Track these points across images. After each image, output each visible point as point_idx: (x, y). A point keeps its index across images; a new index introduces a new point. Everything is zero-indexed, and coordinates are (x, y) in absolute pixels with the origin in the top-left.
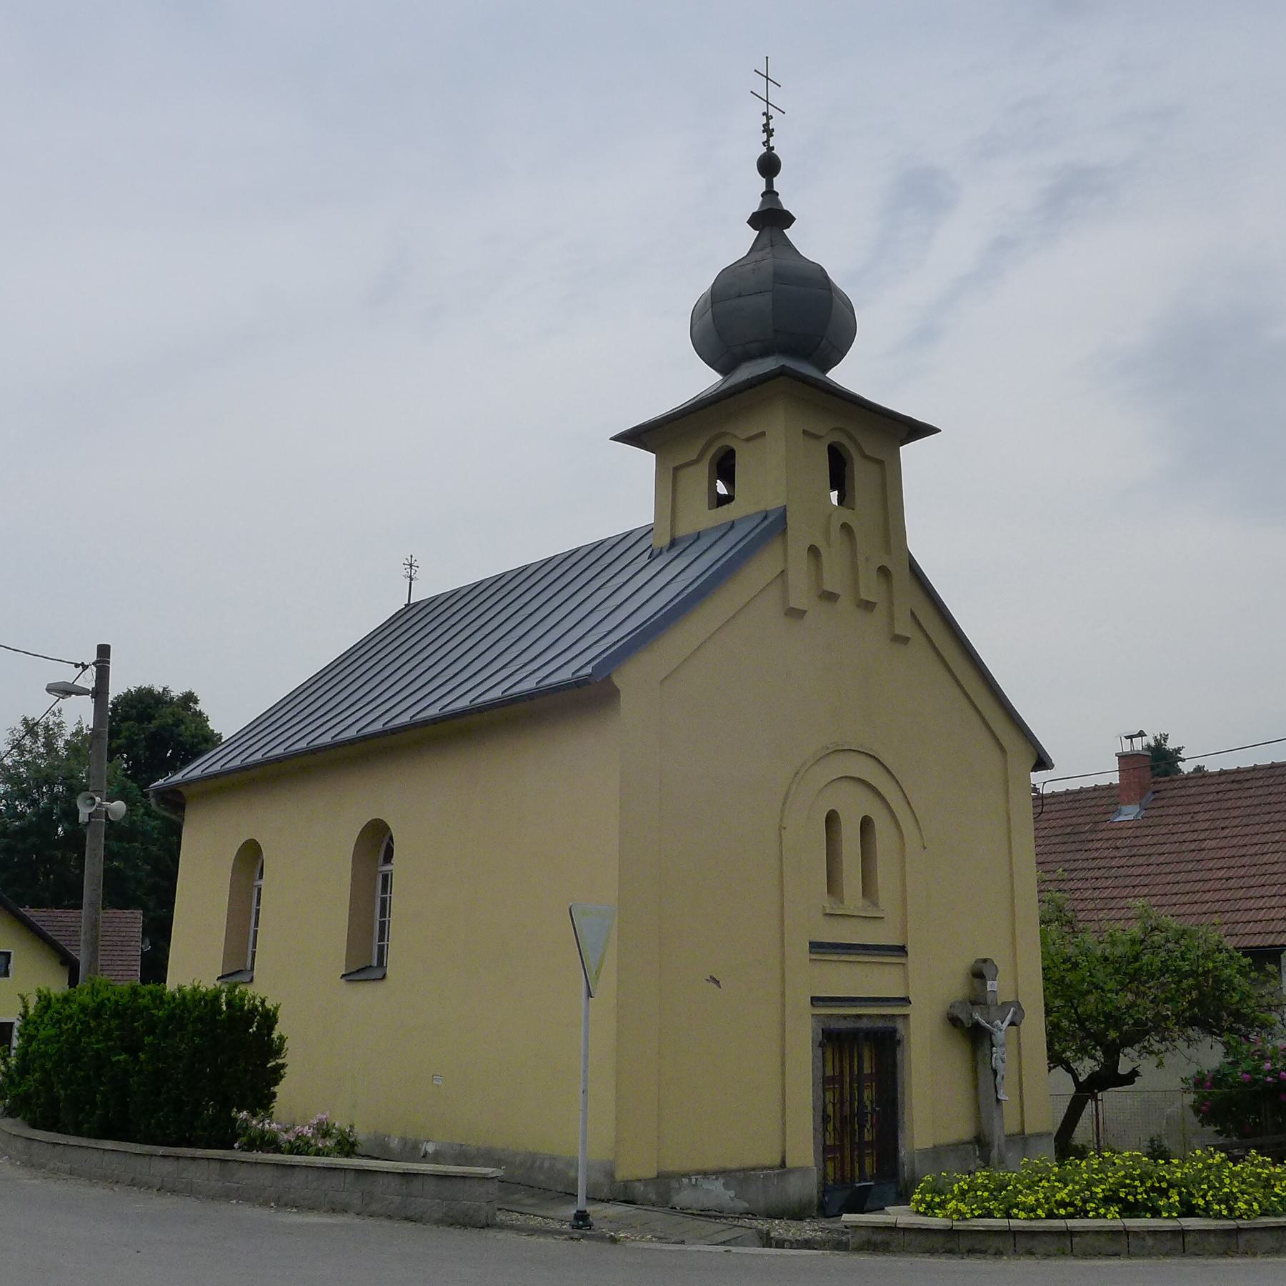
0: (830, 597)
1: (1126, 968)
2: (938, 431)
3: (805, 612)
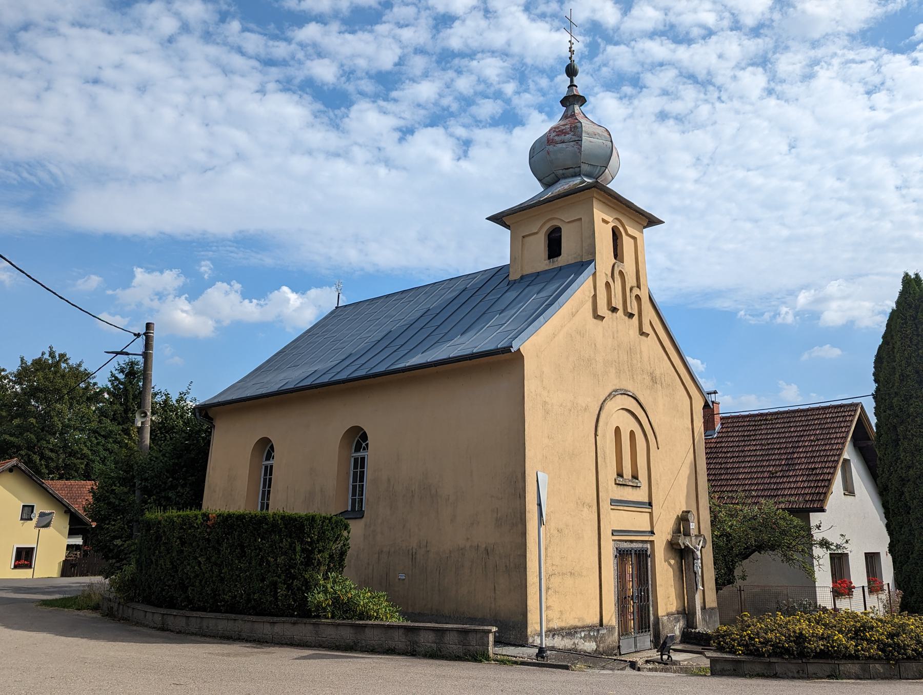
0: (614, 310)
1: (181, 595)
2: (487, 219)
3: (604, 317)
